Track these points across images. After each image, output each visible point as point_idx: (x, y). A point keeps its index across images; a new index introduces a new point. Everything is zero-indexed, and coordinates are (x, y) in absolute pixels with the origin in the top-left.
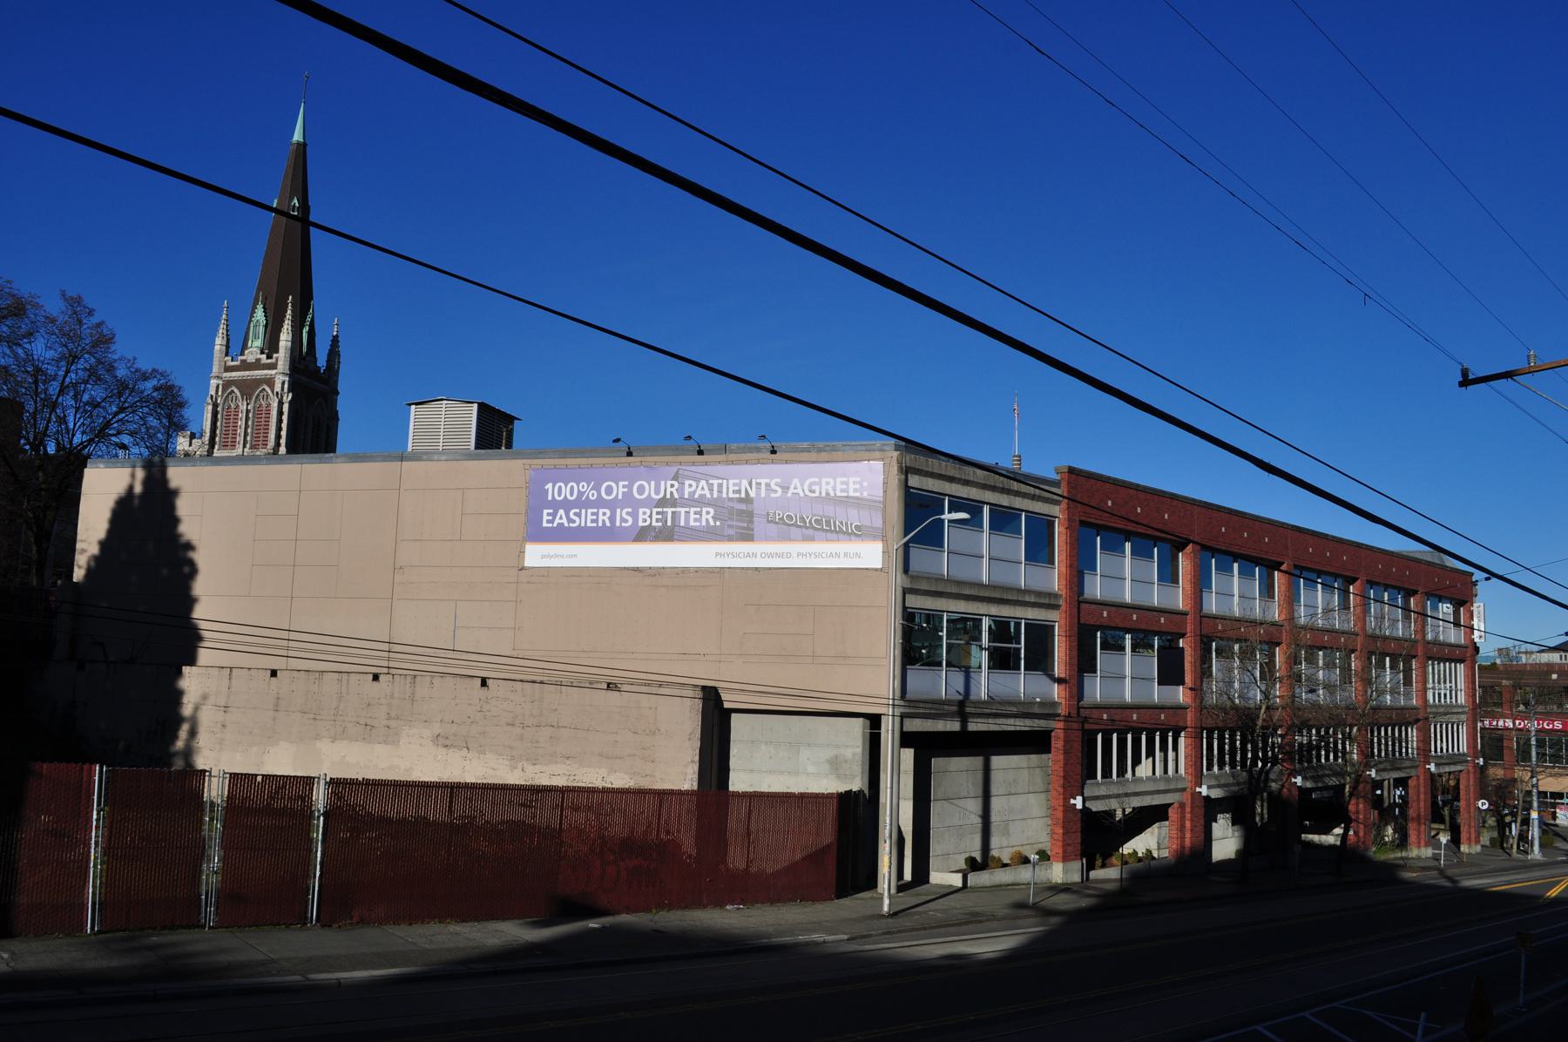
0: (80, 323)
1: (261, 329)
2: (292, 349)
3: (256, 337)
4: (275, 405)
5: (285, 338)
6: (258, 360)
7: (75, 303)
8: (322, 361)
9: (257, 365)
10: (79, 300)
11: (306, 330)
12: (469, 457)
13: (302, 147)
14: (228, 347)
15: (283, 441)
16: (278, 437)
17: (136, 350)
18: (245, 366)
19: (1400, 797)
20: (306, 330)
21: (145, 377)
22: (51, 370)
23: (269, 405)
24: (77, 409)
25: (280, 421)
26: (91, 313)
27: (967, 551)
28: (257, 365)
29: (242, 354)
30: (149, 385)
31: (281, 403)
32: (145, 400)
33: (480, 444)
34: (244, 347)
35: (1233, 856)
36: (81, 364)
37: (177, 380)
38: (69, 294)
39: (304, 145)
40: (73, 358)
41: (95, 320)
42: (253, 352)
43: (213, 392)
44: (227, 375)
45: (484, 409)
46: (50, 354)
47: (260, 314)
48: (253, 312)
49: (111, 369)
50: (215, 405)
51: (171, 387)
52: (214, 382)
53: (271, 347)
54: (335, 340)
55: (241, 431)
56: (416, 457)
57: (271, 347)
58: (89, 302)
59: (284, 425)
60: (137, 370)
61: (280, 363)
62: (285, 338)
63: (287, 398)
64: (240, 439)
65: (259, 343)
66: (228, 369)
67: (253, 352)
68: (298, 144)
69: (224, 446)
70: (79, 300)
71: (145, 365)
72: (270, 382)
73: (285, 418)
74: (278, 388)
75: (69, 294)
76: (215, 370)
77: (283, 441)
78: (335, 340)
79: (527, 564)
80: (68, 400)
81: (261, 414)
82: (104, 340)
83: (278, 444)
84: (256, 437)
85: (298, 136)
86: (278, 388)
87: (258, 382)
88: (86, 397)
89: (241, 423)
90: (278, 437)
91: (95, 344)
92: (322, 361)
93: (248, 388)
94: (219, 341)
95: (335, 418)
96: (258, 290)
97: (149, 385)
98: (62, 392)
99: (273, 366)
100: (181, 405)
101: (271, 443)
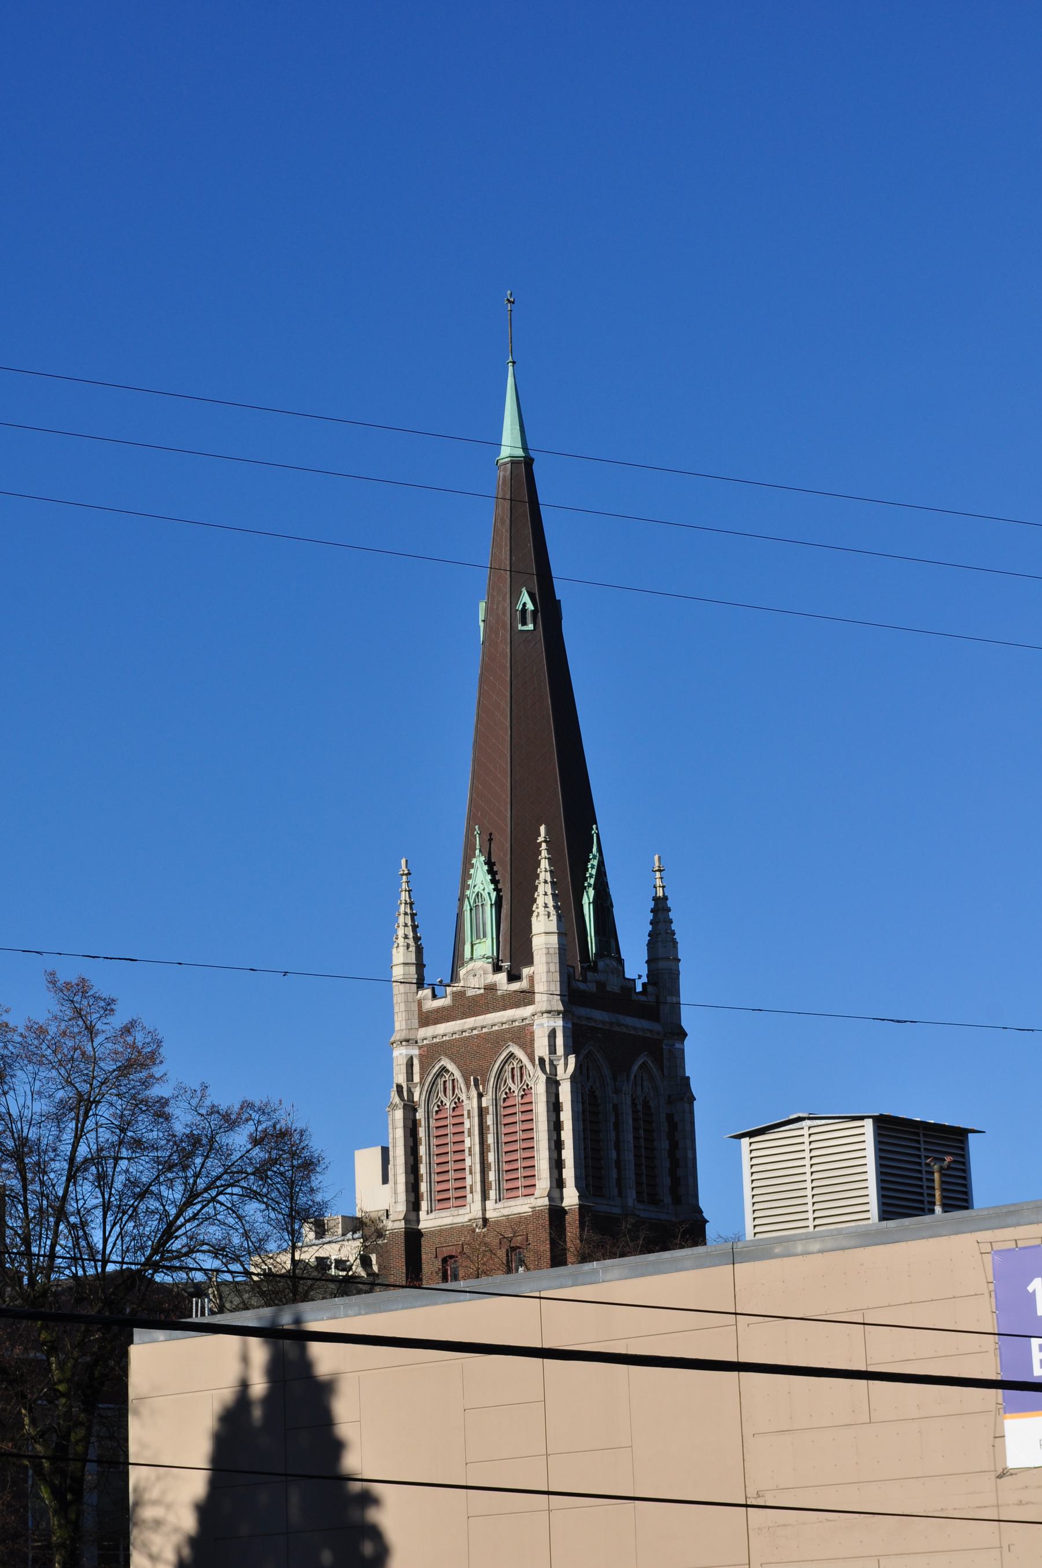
0: (91, 1031)
1: (489, 914)
2: (563, 951)
3: (479, 934)
4: (540, 1089)
5: (544, 928)
7: (77, 996)
8: (636, 966)
9: (490, 1000)
10: (82, 987)
11: (588, 897)
12: (866, 1238)
13: (524, 468)
14: (420, 966)
15: (569, 1173)
16: (557, 1164)
17: (204, 1073)
18: (467, 1006)
20: (588, 897)
21: (230, 1122)
22: (46, 1134)
23: (526, 1091)
24: (106, 1207)
25: (556, 1126)
26: (108, 1007)
28: (490, 1000)
29: (454, 977)
30: (238, 1140)
31: (553, 1084)
32: (233, 1174)
33: (885, 1214)
34: (457, 960)
36: (104, 1112)
37: (295, 1115)
38: (62, 978)
39: (528, 462)
40: (83, 1105)
41: (118, 1020)
42: (478, 973)
43: (400, 1078)
44: (427, 1033)
45: (891, 1130)
46: (41, 1106)
47: (480, 879)
48: (466, 876)
49: (160, 1112)
50: (410, 1109)
51: (284, 1134)
52: (400, 1054)
53: (515, 954)
54: (660, 908)
55: (472, 1161)
56: (761, 1251)
57: (515, 954)
58: (101, 987)
59: (567, 1135)
60: (214, 1110)
61: (540, 987)
62: (544, 928)
63: (566, 1069)
64: (473, 1180)
65: (486, 947)
66: (427, 1019)
67: (478, 973)
68: (514, 462)
69: (442, 1201)
70: (82, 987)
71: (226, 1098)
72: (523, 1035)
73: (566, 1116)
74: (541, 1048)
75: (62, 978)
76: (400, 1024)
77: (569, 1173)
78: (660, 908)
79: (1011, 1463)
80: (87, 1194)
81: (510, 1113)
82: (139, 1061)
83: (558, 1183)
84: (507, 1172)
86: (541, 1048)
87: (496, 1040)
88: (119, 1181)
89: (471, 1142)
90: (557, 1164)
91: (125, 1069)
92: (636, 966)
93: (478, 1057)
95: (681, 1095)
96: (472, 819)
97: (238, 1140)
98: (71, 1177)
99: (526, 997)
100: (309, 1166)
101: (543, 1183)
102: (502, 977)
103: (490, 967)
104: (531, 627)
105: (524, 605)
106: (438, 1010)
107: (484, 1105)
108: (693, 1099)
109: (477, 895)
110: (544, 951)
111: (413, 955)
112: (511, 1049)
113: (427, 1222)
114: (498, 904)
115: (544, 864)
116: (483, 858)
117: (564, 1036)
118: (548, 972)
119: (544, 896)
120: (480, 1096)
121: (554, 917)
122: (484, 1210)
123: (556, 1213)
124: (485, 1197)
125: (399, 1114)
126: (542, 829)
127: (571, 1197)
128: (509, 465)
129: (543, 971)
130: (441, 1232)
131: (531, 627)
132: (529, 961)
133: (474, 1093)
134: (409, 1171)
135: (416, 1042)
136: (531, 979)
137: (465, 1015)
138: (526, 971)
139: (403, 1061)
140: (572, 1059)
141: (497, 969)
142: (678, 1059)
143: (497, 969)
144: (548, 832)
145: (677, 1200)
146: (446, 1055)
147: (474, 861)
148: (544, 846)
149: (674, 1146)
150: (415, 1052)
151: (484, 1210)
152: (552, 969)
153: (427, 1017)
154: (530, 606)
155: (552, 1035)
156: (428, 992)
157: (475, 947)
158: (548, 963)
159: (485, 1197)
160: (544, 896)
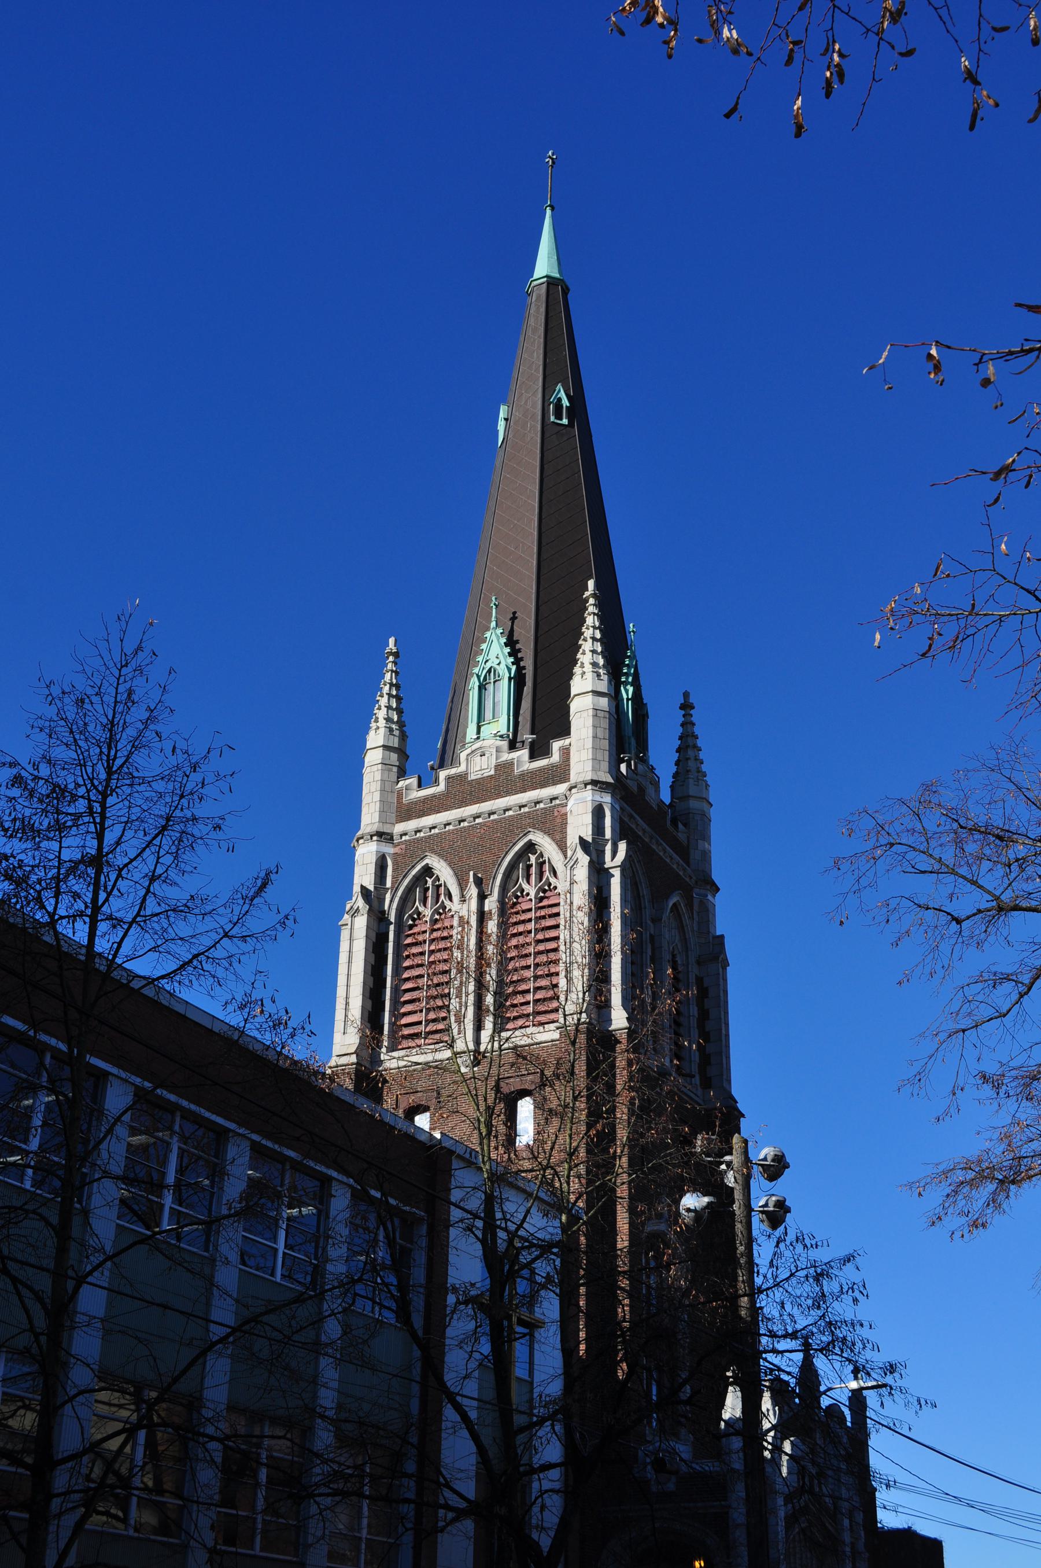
1: (502, 693)
6: (504, 768)
14: (402, 752)
18: (466, 791)
19: (85, 1167)
27: (938, 1448)
28: (503, 781)
31: (599, 874)
35: (519, 1102)
42: (486, 741)
52: (366, 853)
53: (544, 717)
57: (544, 717)
62: (586, 685)
63: (616, 857)
65: (501, 724)
67: (486, 741)
68: (551, 282)
72: (553, 821)
76: (370, 817)
85: (545, 265)
94: (376, 737)
99: (559, 774)
101: (574, 997)
102: (524, 753)
103: (505, 744)
104: (565, 421)
105: (560, 400)
106: (425, 800)
107: (486, 909)
108: (726, 964)
109: (489, 671)
110: (591, 712)
111: (396, 740)
112: (530, 837)
113: (392, 1061)
114: (518, 680)
115: (590, 620)
116: (499, 631)
117: (612, 817)
118: (595, 737)
119: (589, 653)
120: (482, 897)
121: (605, 678)
122: (477, 1041)
123: (598, 1039)
124: (479, 1027)
125: (361, 922)
126: (591, 584)
127: (619, 1019)
128: (545, 285)
129: (583, 744)
130: (407, 1074)
131: (565, 421)
132: (564, 731)
133: (473, 891)
134: (368, 995)
135: (392, 839)
136: (566, 752)
137: (463, 803)
138: (556, 745)
139: (373, 859)
140: (622, 846)
141: (513, 746)
142: (706, 914)
143: (513, 746)
144: (597, 586)
145: (707, 1083)
146: (433, 851)
147: (488, 635)
148: (592, 601)
149: (704, 1015)
150: (389, 849)
151: (477, 1041)
152: (600, 735)
153: (408, 810)
154: (565, 402)
155: (598, 813)
156: (413, 781)
157: (482, 729)
158: (594, 727)
159: (479, 1027)
160: (589, 653)
